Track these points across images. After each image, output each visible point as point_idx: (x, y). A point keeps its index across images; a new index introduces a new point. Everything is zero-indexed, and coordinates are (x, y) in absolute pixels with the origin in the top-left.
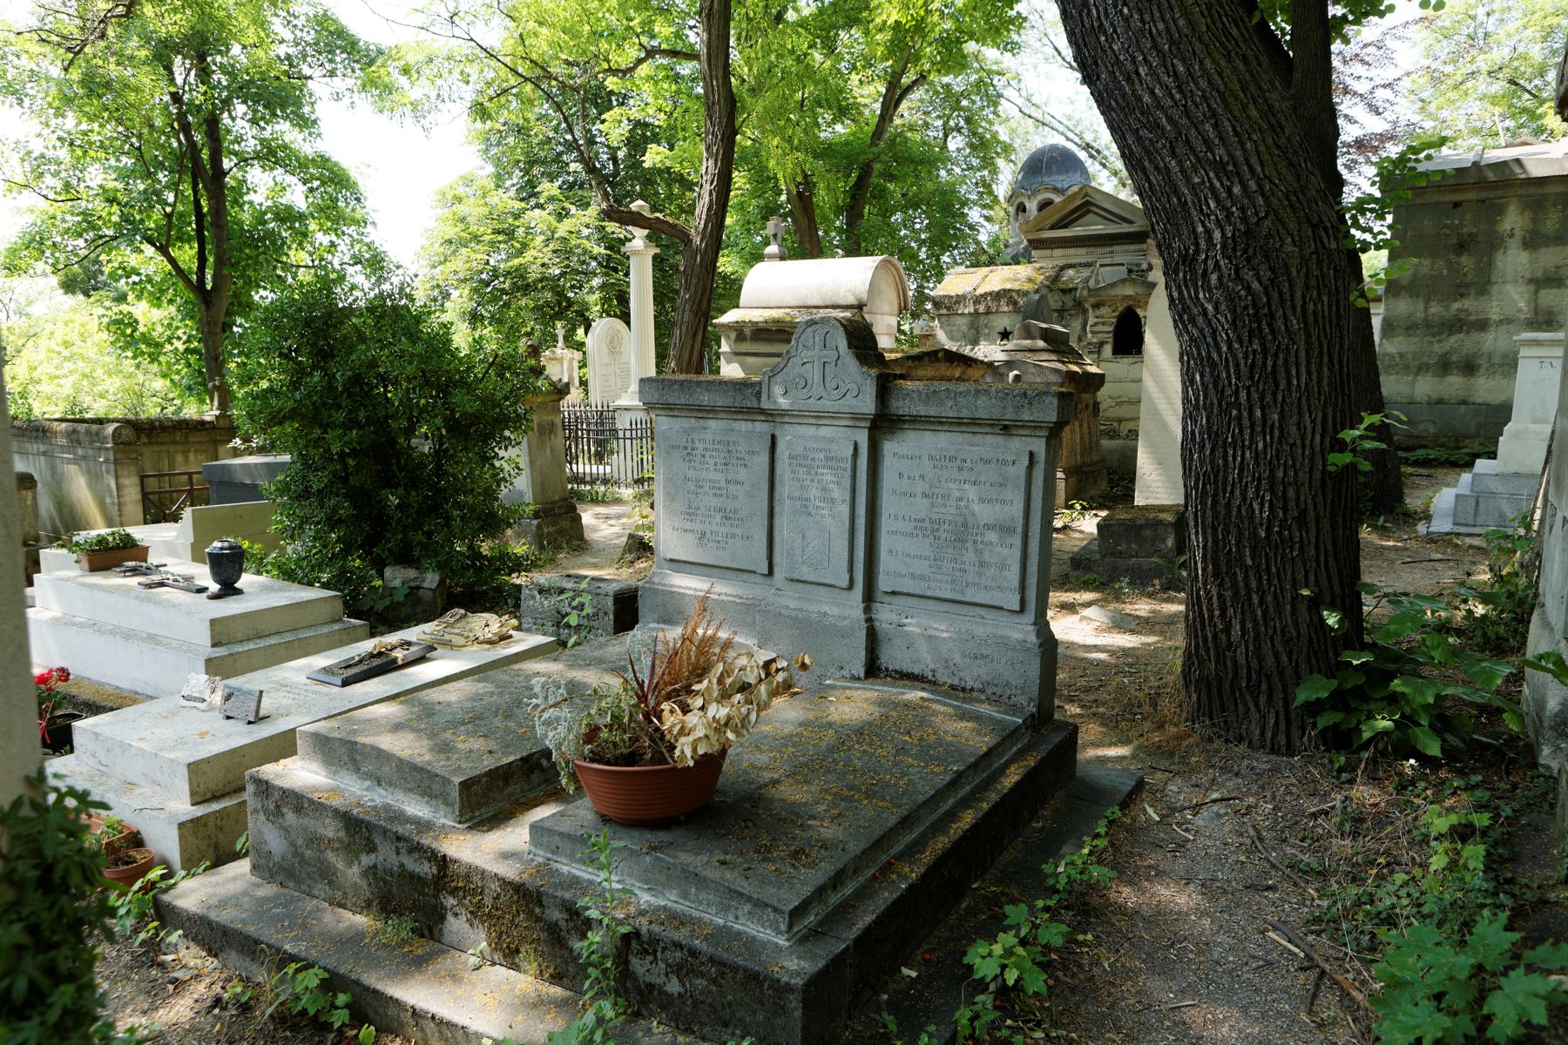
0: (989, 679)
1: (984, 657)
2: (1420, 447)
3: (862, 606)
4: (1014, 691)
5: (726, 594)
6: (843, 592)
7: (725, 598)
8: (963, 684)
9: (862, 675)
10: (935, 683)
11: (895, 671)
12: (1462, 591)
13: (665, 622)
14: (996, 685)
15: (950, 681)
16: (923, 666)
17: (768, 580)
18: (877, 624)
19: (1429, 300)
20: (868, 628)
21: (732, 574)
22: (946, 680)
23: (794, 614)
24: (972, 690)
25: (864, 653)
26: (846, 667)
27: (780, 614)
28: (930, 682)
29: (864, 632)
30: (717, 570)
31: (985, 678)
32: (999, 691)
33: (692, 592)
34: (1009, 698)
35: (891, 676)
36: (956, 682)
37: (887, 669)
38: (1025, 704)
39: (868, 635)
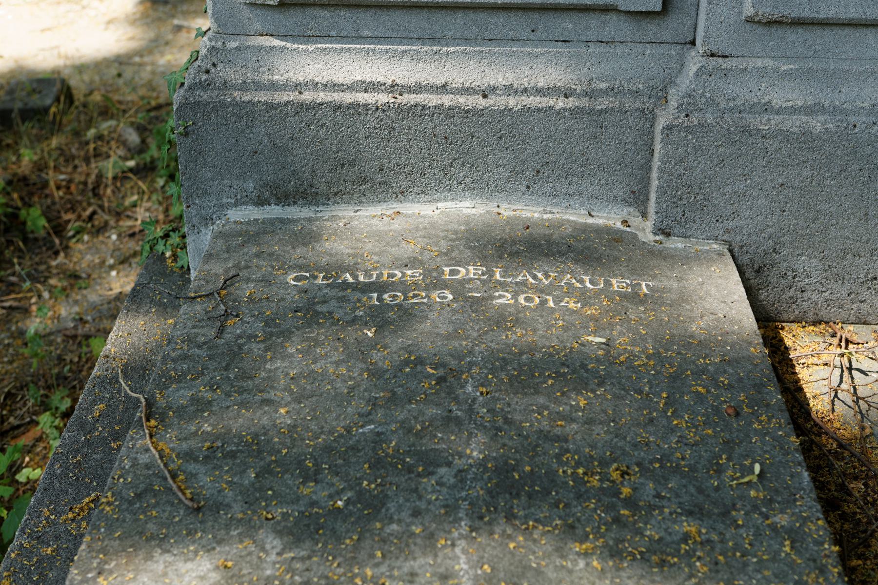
5: (510, 90)
7: (512, 102)
13: (285, 198)
17: (668, 29)
21: (516, 20)
23: (795, 123)
27: (746, 130)
30: (460, 18)
33: (383, 98)
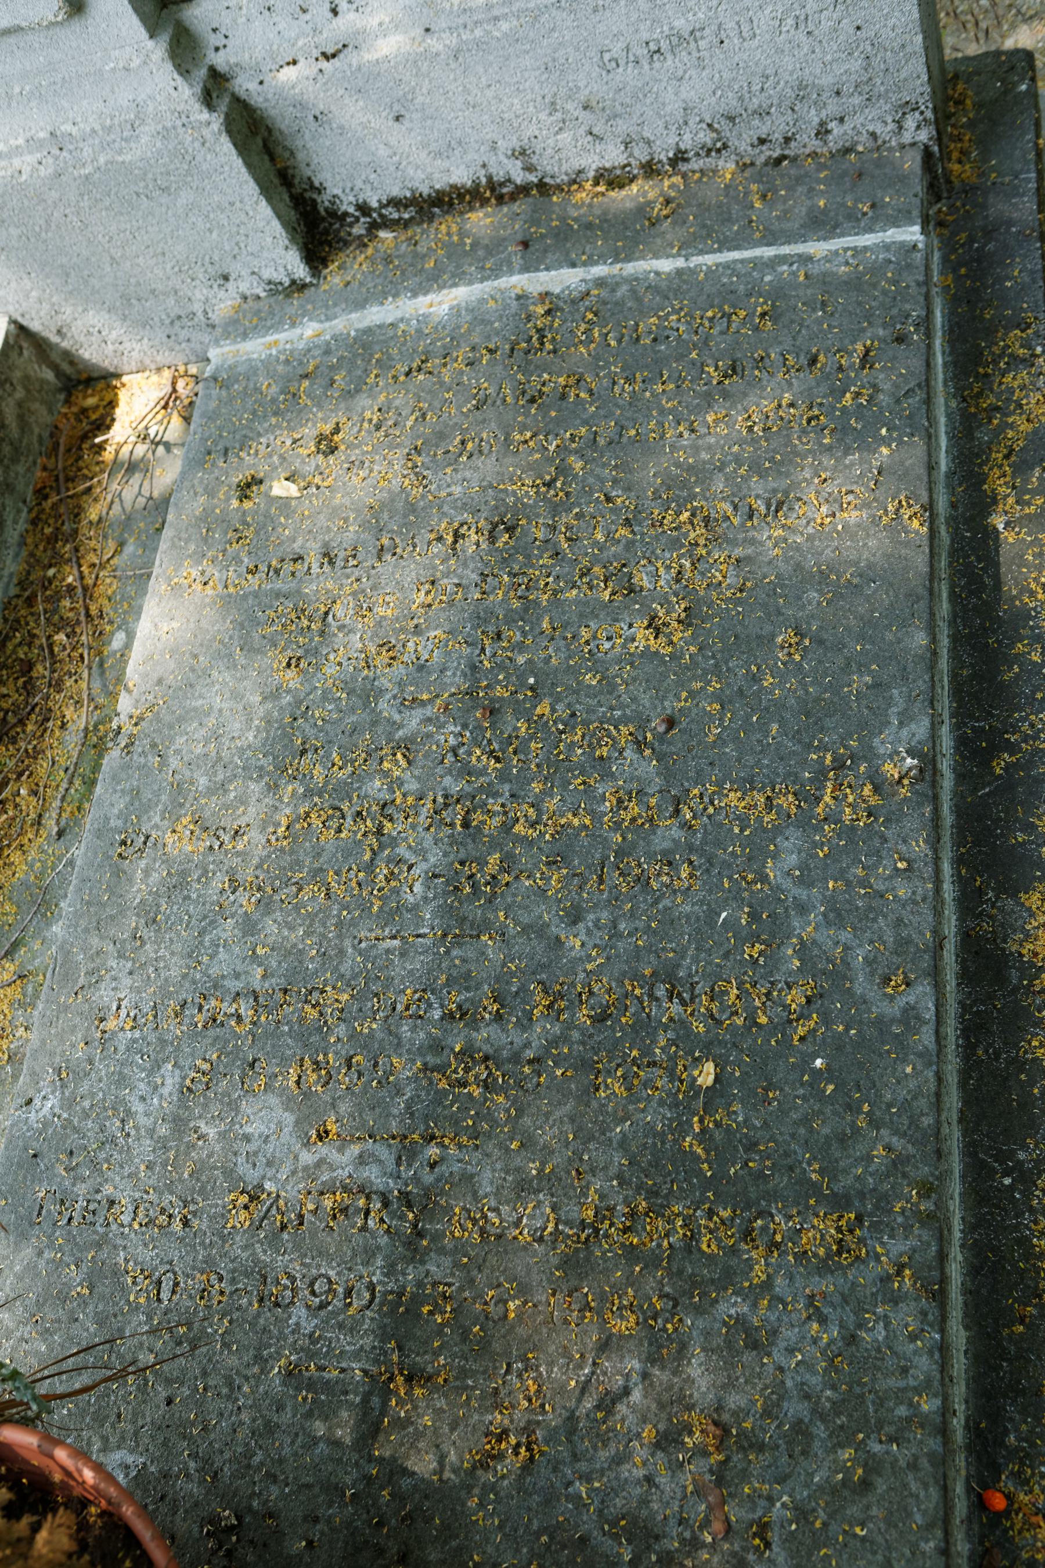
0: (731, 102)
1: (680, 40)
2: (90, 675)
3: (157, 50)
4: (833, 107)
6: (60, 33)
8: (641, 154)
9: (301, 271)
10: (542, 186)
11: (395, 202)
12: (41, 789)
14: (762, 113)
15: (592, 162)
16: (477, 155)
18: (245, 85)
19: (115, 461)
20: (230, 128)
22: (576, 163)
24: (679, 157)
25: (265, 209)
26: (235, 268)
28: (524, 190)
29: (226, 145)
31: (710, 106)
32: (777, 126)
34: (822, 132)
35: (386, 223)
36: (613, 156)
37: (364, 209)
38: (884, 131)
39: (242, 148)
